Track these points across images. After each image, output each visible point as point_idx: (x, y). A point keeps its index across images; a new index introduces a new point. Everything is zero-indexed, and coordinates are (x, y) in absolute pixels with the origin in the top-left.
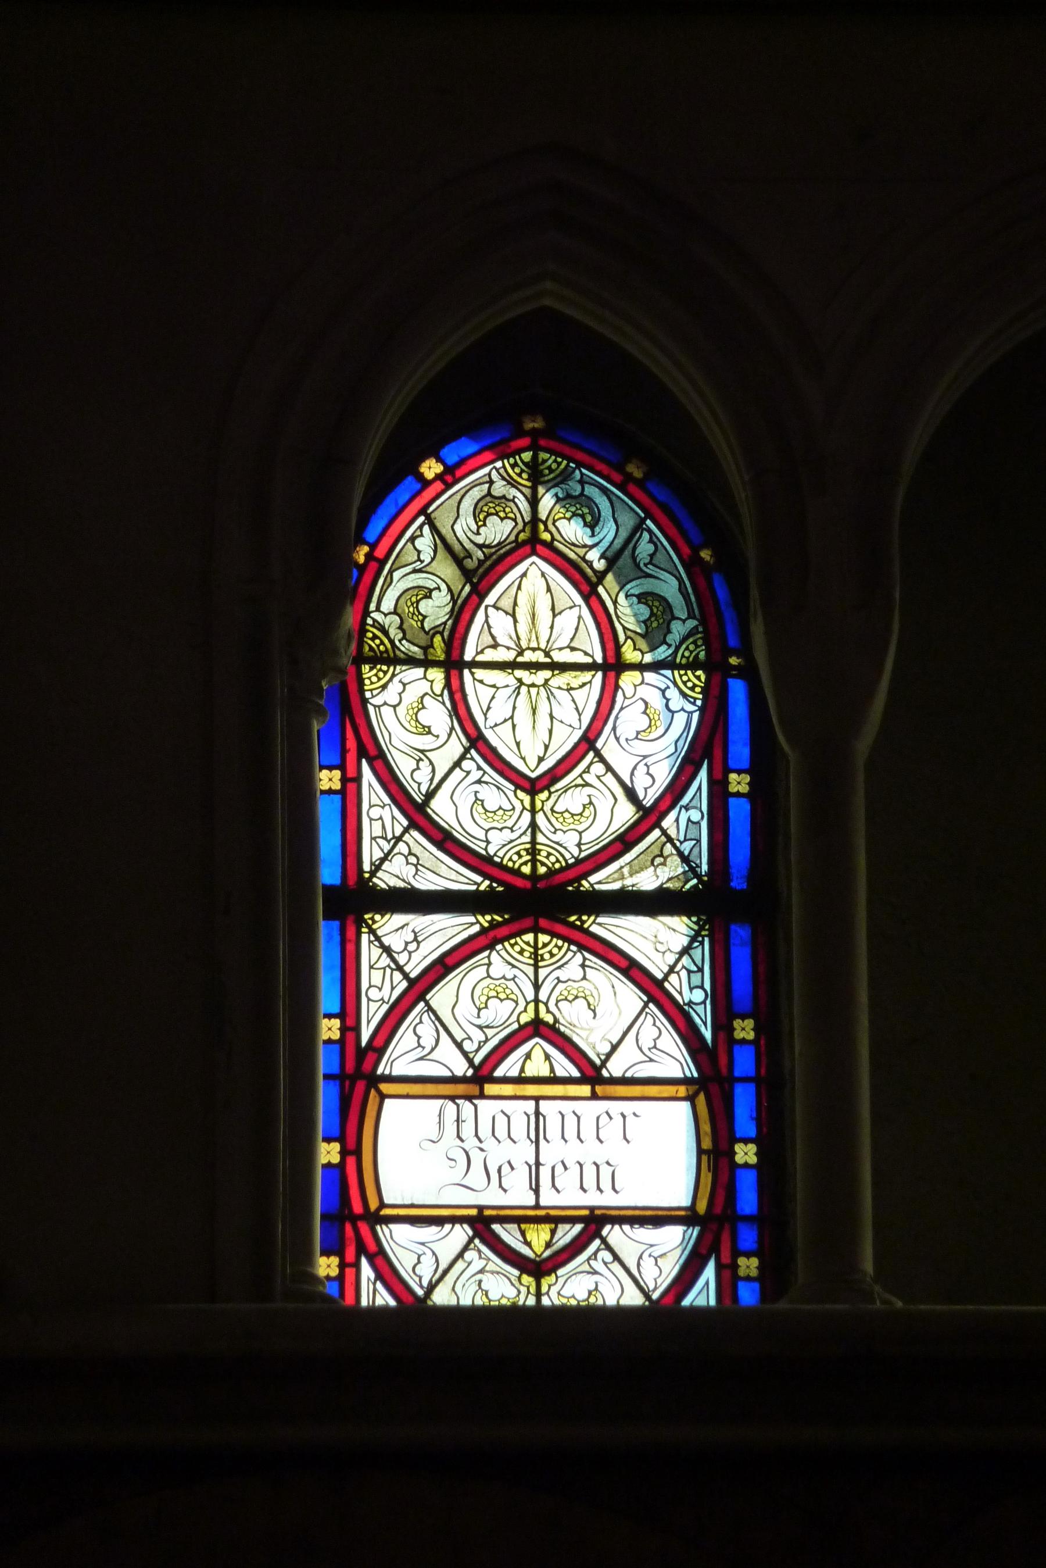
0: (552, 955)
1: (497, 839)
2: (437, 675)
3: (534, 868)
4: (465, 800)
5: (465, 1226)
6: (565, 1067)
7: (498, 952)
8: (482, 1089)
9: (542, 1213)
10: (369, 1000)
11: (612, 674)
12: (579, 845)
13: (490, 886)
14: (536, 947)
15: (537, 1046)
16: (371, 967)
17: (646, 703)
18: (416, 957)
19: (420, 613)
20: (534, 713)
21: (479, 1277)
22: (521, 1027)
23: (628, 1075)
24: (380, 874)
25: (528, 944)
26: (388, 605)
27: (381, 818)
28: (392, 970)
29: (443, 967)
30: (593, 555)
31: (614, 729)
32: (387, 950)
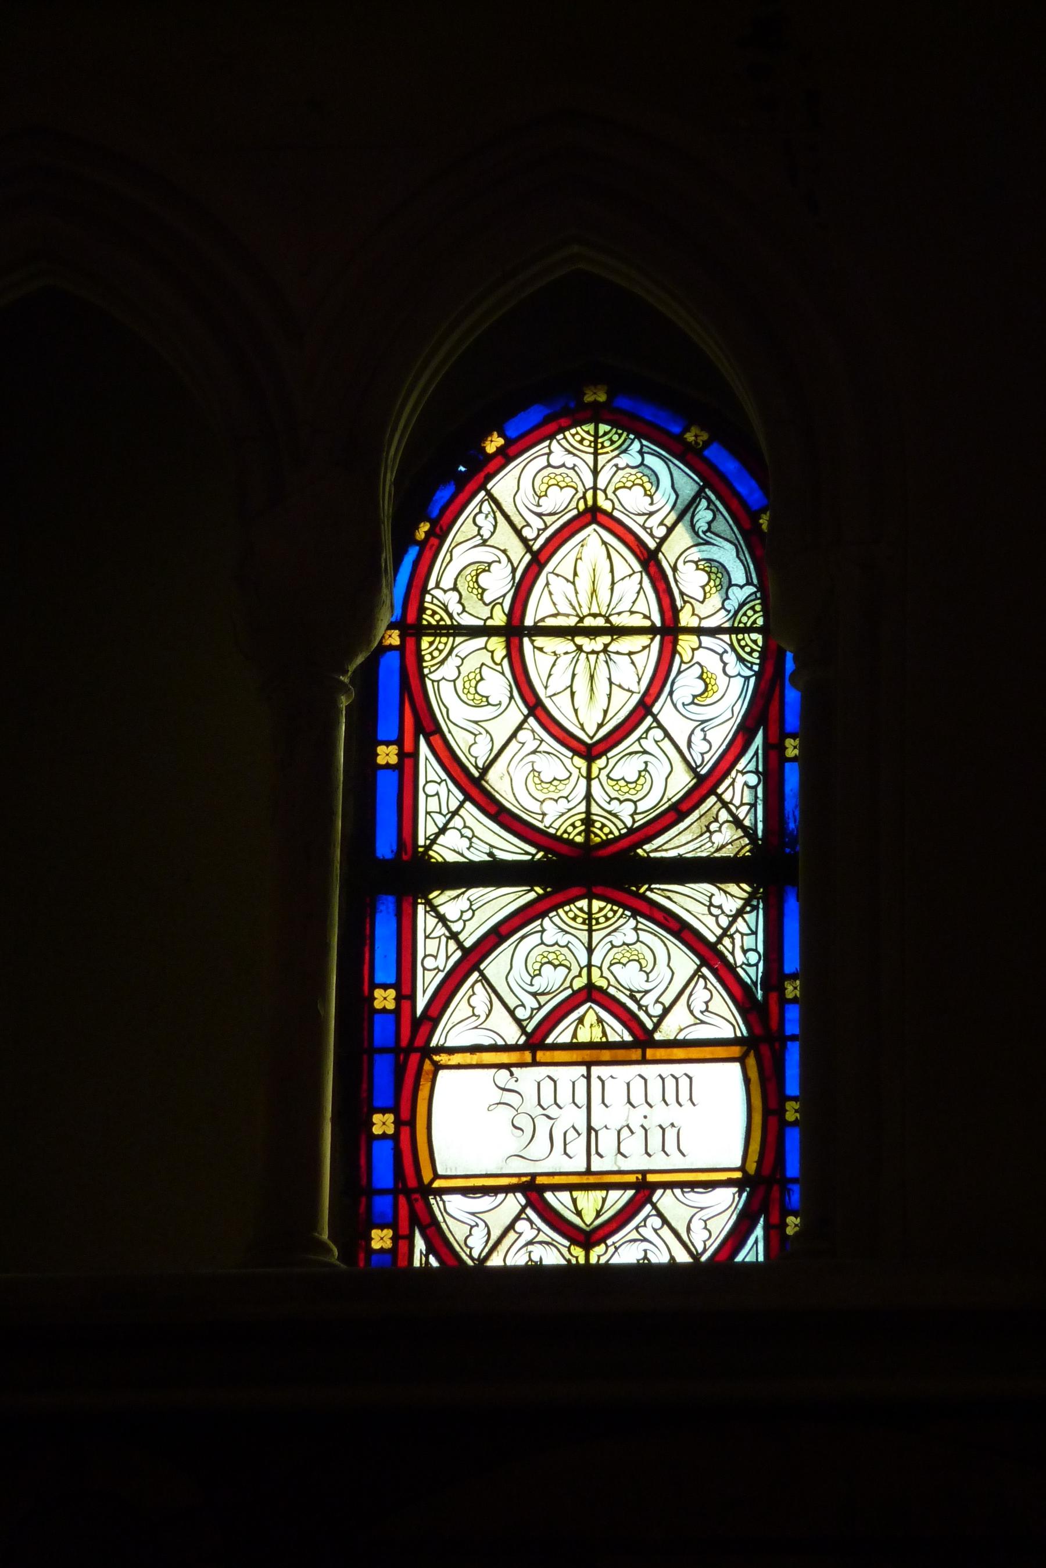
0: (607, 919)
1: (552, 810)
2: (497, 644)
3: (587, 838)
4: (520, 773)
5: (519, 1195)
6: (618, 1032)
7: (550, 919)
8: (534, 1057)
9: (592, 1179)
10: (424, 969)
11: (669, 638)
12: (543, 931)
13: (639, 888)
14: (590, 913)
15: (591, 1012)
16: (427, 937)
17: (482, 599)
18: (471, 926)
19: (479, 587)
20: (594, 591)
21: (653, 508)
22: (604, 753)
23: (680, 1037)
24: (435, 847)
25: (581, 910)
26: (447, 583)
27: (437, 794)
28: (448, 938)
29: (497, 935)
30: (529, 1234)
31: (671, 693)
32: (442, 919)
